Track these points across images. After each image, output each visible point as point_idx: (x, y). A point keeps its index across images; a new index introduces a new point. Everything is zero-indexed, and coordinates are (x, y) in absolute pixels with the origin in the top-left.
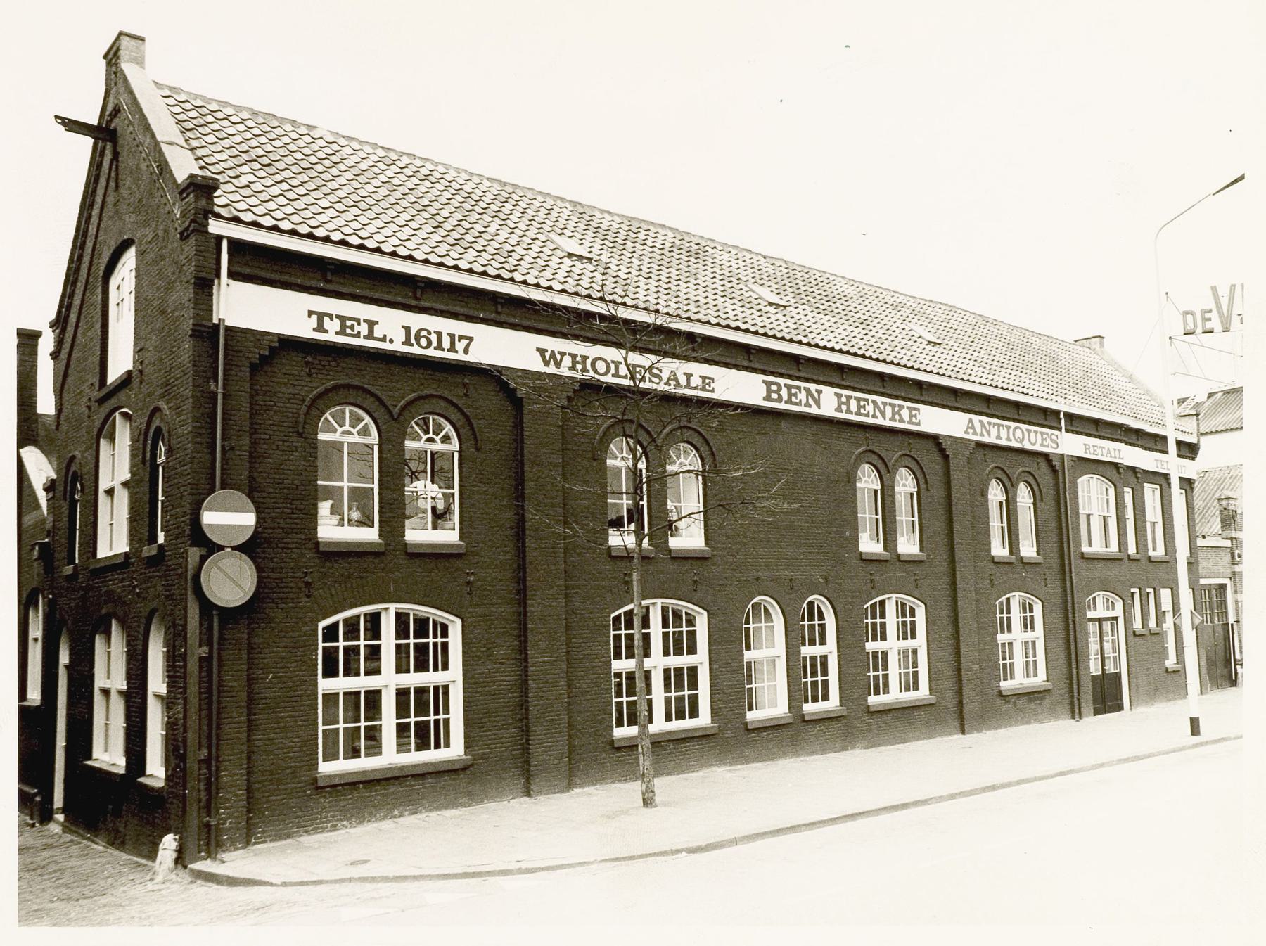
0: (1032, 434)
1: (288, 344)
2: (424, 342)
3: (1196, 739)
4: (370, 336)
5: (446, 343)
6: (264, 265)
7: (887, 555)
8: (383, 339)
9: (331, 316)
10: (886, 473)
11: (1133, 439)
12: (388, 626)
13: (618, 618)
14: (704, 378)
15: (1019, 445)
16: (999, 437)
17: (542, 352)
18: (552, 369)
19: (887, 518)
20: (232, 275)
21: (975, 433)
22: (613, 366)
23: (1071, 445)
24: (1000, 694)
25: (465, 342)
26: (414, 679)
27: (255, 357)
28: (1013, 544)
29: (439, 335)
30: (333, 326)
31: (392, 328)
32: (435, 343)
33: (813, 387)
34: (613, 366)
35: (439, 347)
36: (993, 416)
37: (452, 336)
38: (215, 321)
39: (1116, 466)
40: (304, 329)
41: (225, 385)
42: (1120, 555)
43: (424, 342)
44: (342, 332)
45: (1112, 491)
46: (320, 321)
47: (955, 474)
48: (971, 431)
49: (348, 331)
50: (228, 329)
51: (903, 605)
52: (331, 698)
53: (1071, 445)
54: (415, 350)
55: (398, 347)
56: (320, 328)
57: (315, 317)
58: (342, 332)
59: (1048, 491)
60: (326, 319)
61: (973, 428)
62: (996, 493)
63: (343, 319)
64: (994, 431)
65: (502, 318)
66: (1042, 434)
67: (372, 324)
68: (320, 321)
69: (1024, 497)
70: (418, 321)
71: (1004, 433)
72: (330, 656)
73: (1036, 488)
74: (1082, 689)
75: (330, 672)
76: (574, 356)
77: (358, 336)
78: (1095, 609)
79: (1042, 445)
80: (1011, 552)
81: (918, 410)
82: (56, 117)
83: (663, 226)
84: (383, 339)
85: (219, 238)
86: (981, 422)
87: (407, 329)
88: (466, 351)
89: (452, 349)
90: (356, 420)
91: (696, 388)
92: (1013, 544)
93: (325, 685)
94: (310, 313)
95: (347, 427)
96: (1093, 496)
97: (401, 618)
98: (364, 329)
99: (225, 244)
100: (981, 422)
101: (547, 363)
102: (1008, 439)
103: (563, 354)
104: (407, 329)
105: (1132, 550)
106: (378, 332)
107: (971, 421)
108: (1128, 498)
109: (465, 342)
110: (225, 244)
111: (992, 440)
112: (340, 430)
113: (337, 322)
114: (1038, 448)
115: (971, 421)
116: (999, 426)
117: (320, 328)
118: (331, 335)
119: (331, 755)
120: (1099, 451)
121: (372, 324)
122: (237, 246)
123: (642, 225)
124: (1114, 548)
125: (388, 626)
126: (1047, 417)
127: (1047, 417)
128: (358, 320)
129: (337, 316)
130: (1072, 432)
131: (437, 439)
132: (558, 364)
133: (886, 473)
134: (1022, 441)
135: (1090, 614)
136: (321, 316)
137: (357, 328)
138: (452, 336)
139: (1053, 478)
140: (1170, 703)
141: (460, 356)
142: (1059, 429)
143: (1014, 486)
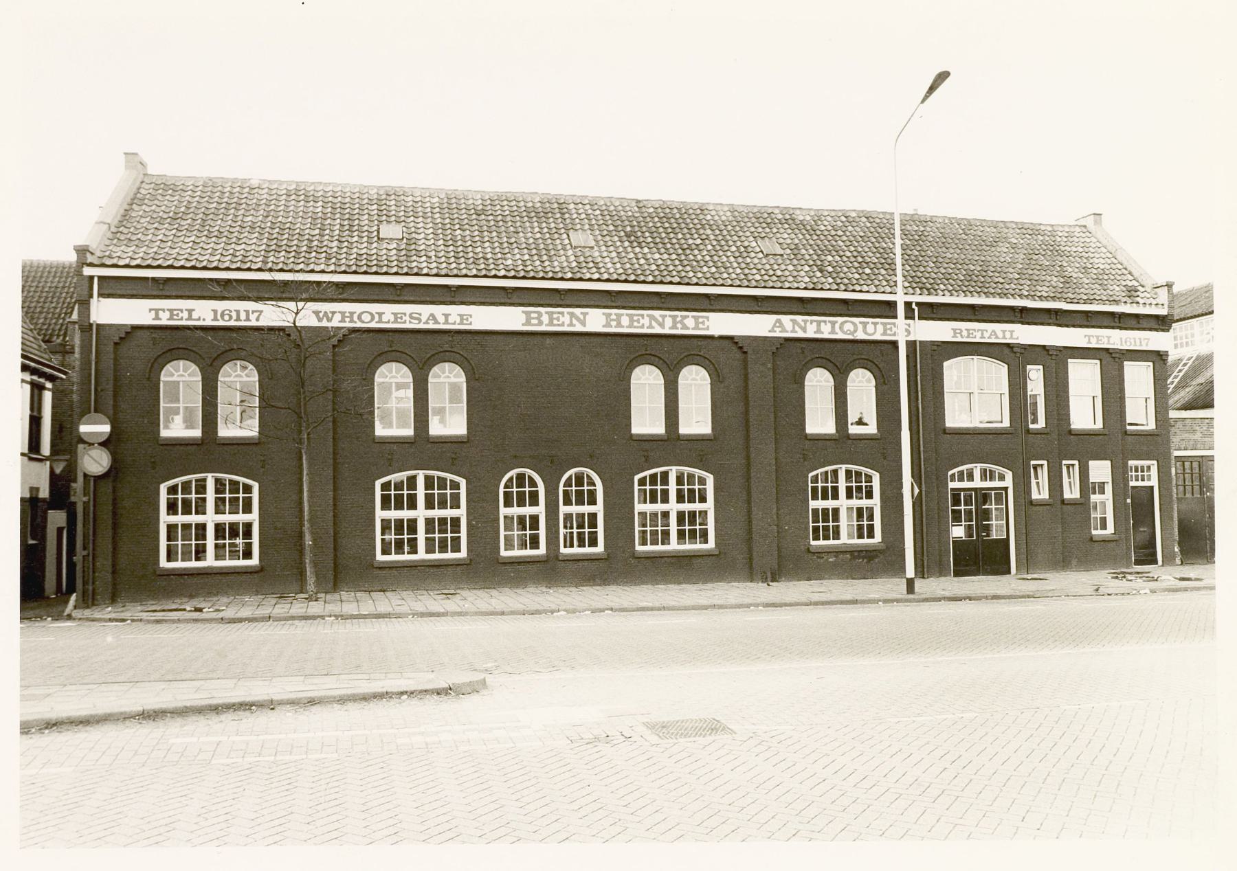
2: (227, 318)
3: (911, 596)
4: (190, 318)
5: (243, 316)
8: (199, 319)
9: (163, 310)
12: (842, 476)
13: (953, 475)
14: (395, 314)
15: (850, 337)
17: (317, 313)
18: (325, 324)
19: (671, 404)
20: (100, 295)
24: (1091, 539)
25: (256, 314)
26: (687, 507)
27: (116, 339)
29: (238, 312)
31: (204, 312)
32: (234, 317)
33: (578, 311)
35: (238, 319)
37: (247, 312)
40: (148, 320)
43: (227, 318)
44: (171, 318)
46: (157, 314)
50: (98, 325)
51: (985, 470)
52: (815, 511)
54: (221, 323)
55: (209, 322)
56: (157, 318)
58: (171, 318)
63: (171, 311)
67: (190, 311)
68: (157, 314)
70: (221, 305)
72: (815, 489)
74: (99, 540)
75: (815, 497)
76: (343, 313)
81: (707, 318)
84: (199, 319)
85: (92, 278)
87: (215, 312)
88: (257, 320)
89: (248, 319)
93: (813, 504)
97: (848, 473)
98: (185, 315)
99: (96, 280)
101: (320, 320)
103: (333, 313)
104: (215, 312)
106: (195, 315)
107: (778, 321)
109: (256, 314)
110: (96, 280)
118: (164, 320)
119: (816, 538)
125: (842, 476)
130: (926, 319)
132: (329, 320)
136: (157, 311)
138: (247, 312)
141: (253, 323)
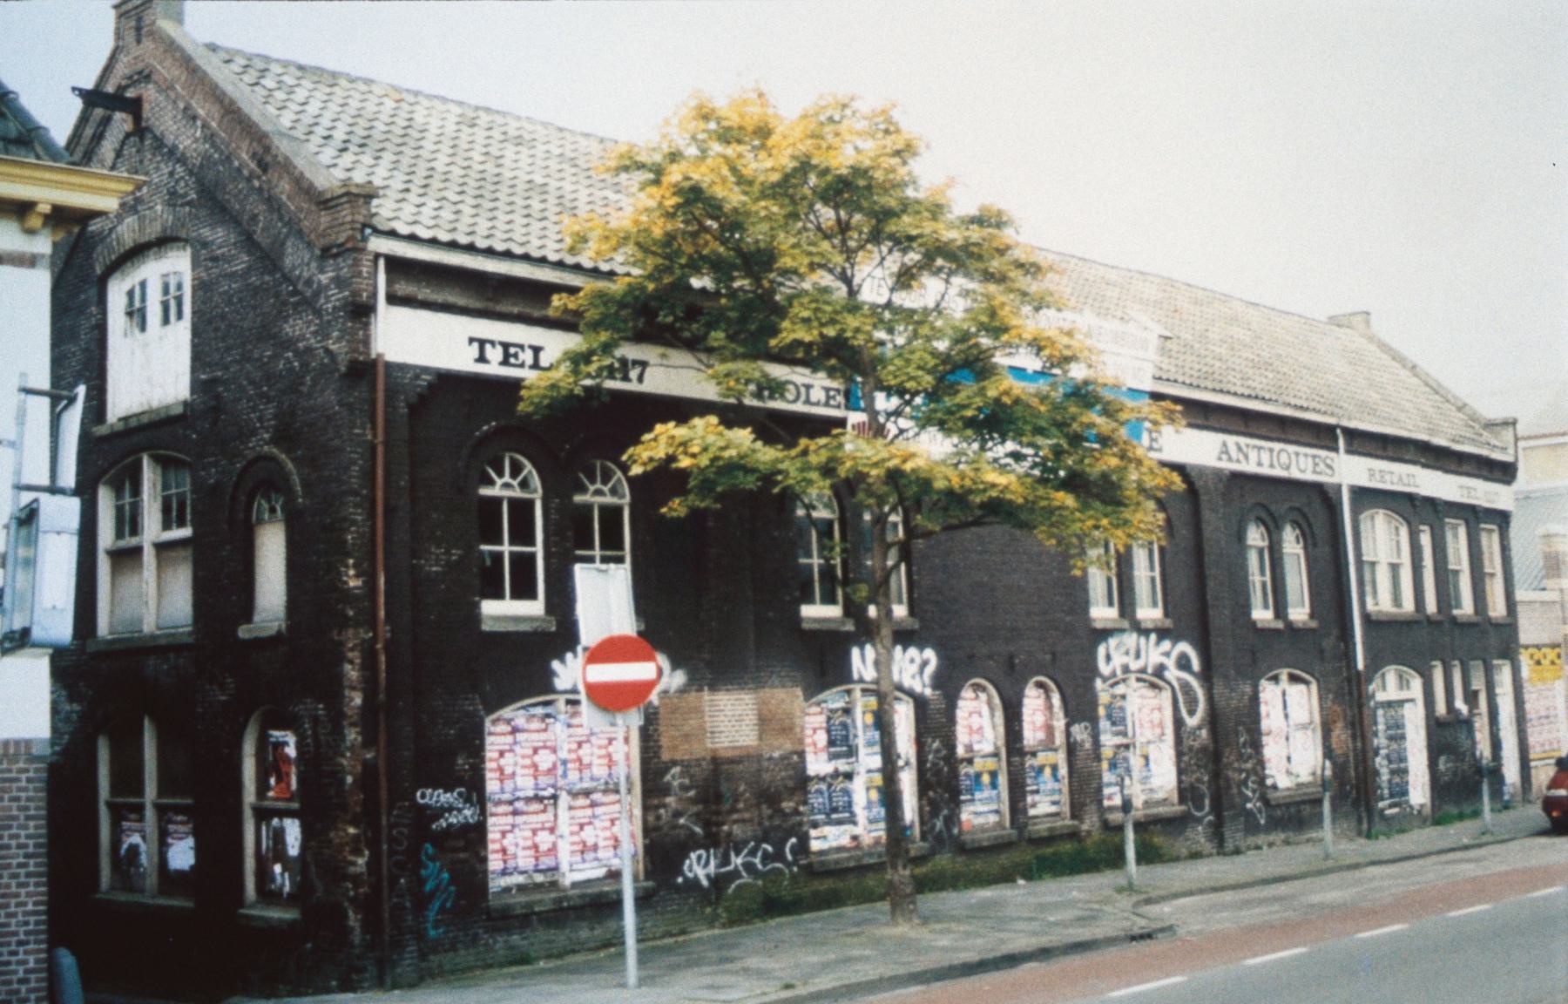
0: (1302, 459)
1: (448, 381)
6: (432, 283)
7: (1280, 625)
9: (493, 343)
10: (1273, 530)
11: (1497, 474)
16: (1260, 464)
21: (1230, 459)
22: (803, 390)
23: (1349, 471)
28: (1280, 610)
30: (494, 354)
34: (803, 390)
36: (1251, 435)
38: (373, 356)
39: (1410, 498)
40: (462, 360)
41: (387, 433)
42: (1419, 617)
45: (1404, 532)
47: (1207, 515)
48: (1224, 457)
49: (512, 360)
53: (1349, 471)
56: (482, 359)
57: (476, 345)
58: (505, 362)
59: (1321, 530)
60: (488, 347)
61: (1227, 452)
62: (1255, 536)
63: (506, 346)
64: (1253, 455)
65: (1250, 430)
66: (1314, 457)
67: (537, 350)
69: (1292, 545)
71: (1265, 457)
73: (1307, 530)
77: (522, 365)
78: (1384, 688)
79: (1314, 472)
80: (1122, 614)
82: (74, 89)
83: (444, 100)
86: (1238, 445)
88: (640, 379)
90: (516, 469)
91: (817, 404)
92: (1280, 610)
94: (471, 340)
95: (507, 479)
96: (1381, 542)
98: (527, 357)
100: (1238, 445)
102: (1272, 466)
105: (1431, 606)
107: (1225, 444)
108: (1425, 539)
110: (382, 263)
111: (1250, 467)
112: (499, 482)
113: (499, 349)
114: (1309, 476)
115: (1225, 444)
116: (1260, 448)
117: (482, 359)
120: (1388, 477)
121: (537, 350)
122: (397, 266)
123: (405, 96)
124: (1408, 605)
126: (1321, 435)
127: (1321, 435)
128: (521, 347)
129: (531, 347)
131: (606, 489)
133: (1273, 530)
134: (1288, 468)
135: (1381, 696)
136: (483, 343)
137: (522, 356)
139: (1317, 511)
140: (386, 996)
142: (1336, 449)
143: (1279, 528)
